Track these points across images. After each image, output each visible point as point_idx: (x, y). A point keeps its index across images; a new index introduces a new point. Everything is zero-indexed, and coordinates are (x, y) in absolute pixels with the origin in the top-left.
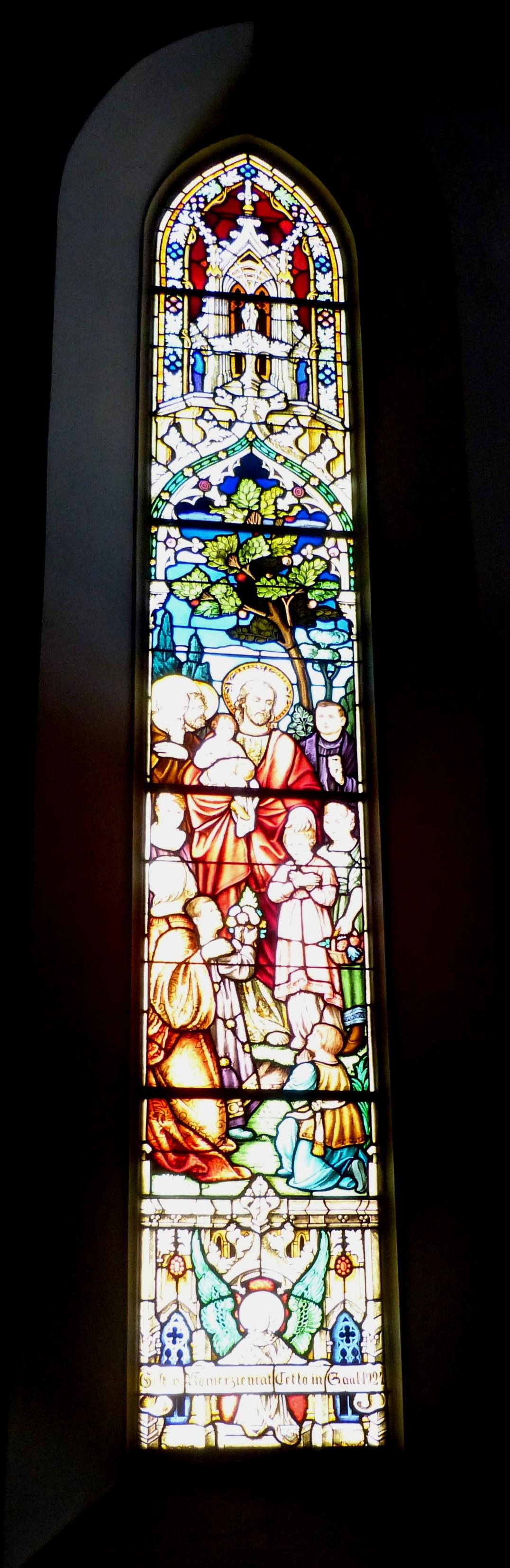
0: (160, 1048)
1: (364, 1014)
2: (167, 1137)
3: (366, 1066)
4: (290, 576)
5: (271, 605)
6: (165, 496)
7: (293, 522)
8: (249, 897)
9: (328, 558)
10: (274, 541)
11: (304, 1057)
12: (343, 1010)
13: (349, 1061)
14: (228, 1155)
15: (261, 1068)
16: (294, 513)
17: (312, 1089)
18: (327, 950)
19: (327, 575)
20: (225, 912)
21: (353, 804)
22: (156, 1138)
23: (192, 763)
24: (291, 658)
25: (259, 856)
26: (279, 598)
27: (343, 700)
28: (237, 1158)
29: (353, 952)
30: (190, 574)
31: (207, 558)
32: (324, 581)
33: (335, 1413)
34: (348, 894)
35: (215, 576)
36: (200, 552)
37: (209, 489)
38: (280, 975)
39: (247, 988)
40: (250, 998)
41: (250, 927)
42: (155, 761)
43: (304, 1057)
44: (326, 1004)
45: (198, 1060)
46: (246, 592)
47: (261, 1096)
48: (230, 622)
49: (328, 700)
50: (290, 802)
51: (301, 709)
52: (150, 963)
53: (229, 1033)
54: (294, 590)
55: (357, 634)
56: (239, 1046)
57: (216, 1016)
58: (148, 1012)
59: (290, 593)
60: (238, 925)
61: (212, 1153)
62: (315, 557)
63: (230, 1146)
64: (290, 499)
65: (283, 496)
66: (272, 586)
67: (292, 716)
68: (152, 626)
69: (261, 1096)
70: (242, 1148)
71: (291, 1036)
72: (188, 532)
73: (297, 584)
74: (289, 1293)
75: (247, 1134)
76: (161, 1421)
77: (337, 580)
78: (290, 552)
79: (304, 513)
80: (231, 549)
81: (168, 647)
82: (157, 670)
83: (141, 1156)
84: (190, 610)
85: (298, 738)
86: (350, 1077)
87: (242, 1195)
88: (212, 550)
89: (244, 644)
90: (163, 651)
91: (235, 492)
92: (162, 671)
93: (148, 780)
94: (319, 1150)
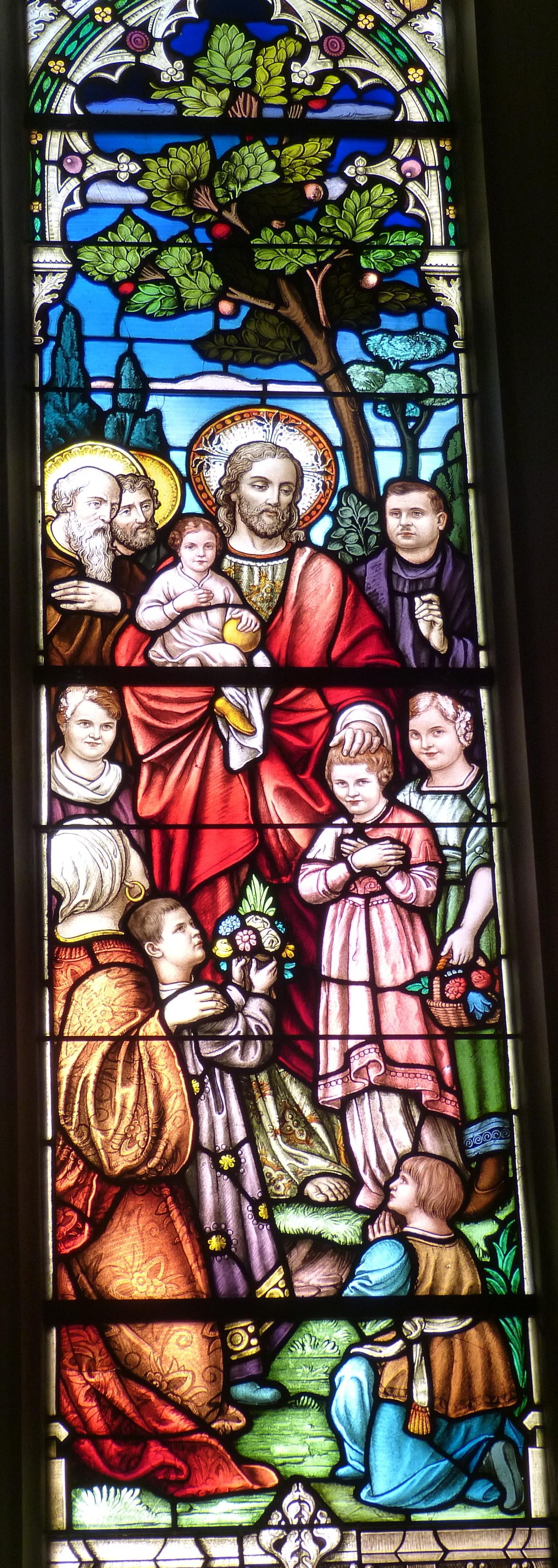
0: (82, 1218)
1: (506, 1132)
2: (99, 1405)
3: (514, 1241)
4: (322, 223)
5: (284, 286)
6: (57, 67)
7: (325, 109)
8: (257, 895)
9: (398, 180)
10: (286, 150)
11: (382, 1227)
12: (460, 1124)
13: (478, 1233)
14: (230, 1440)
15: (294, 1253)
16: (326, 90)
17: (403, 1293)
18: (424, 1000)
19: (400, 216)
20: (209, 928)
21: (467, 693)
22: (78, 1409)
23: (132, 621)
24: (328, 395)
25: (278, 810)
26: (301, 270)
27: (441, 478)
28: (250, 1445)
29: (476, 1000)
30: (114, 228)
31: (148, 192)
32: (393, 229)
34: (465, 881)
35: (165, 229)
36: (133, 181)
37: (149, 49)
38: (331, 1056)
39: (260, 1086)
40: (269, 1108)
41: (261, 957)
42: (55, 618)
43: (382, 1227)
44: (427, 1114)
45: (160, 1242)
46: (231, 258)
47: (297, 1312)
48: (200, 325)
49: (408, 479)
50: (336, 695)
51: (353, 500)
52: (58, 1040)
53: (226, 1184)
54: (330, 252)
55: (465, 338)
56: (247, 1207)
57: (197, 1146)
58: (53, 1143)
59: (323, 258)
60: (237, 953)
61: (197, 1437)
62: (374, 180)
63: (234, 1420)
64: (315, 62)
65: (302, 57)
66: (286, 246)
67: (334, 515)
68: (39, 340)
69: (297, 1312)
70: (261, 1423)
71: (355, 1184)
72: (107, 141)
73: (336, 238)
75: (267, 1394)
77: (422, 226)
78: (319, 173)
79: (347, 90)
80: (198, 171)
81: (73, 382)
82: (52, 431)
83: (47, 1447)
84: (115, 303)
85: (349, 560)
86: (480, 1267)
87: (262, 1524)
88: (157, 177)
89: (232, 369)
90: (63, 390)
91: (203, 51)
92: (62, 432)
93: (41, 659)
94: (418, 1424)
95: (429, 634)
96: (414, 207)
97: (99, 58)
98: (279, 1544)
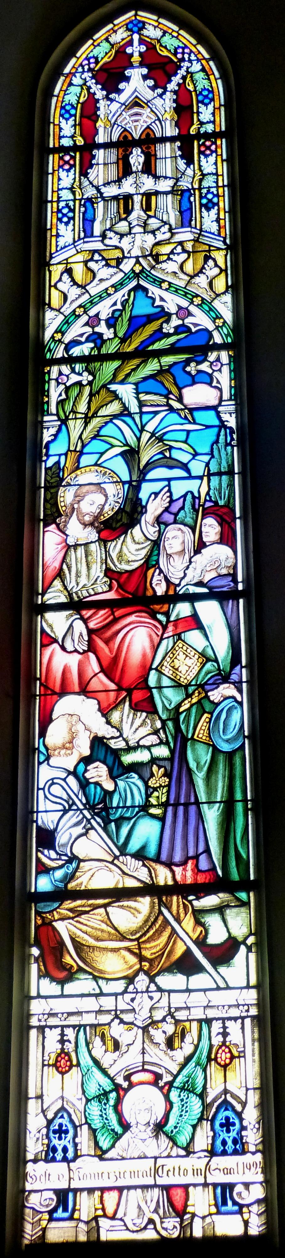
6: (58, 336)
33: (216, 1205)
74: (170, 1084)
76: (46, 1216)
83: (29, 959)
95: (130, 383)
97: (78, 329)
98: (133, 1000)
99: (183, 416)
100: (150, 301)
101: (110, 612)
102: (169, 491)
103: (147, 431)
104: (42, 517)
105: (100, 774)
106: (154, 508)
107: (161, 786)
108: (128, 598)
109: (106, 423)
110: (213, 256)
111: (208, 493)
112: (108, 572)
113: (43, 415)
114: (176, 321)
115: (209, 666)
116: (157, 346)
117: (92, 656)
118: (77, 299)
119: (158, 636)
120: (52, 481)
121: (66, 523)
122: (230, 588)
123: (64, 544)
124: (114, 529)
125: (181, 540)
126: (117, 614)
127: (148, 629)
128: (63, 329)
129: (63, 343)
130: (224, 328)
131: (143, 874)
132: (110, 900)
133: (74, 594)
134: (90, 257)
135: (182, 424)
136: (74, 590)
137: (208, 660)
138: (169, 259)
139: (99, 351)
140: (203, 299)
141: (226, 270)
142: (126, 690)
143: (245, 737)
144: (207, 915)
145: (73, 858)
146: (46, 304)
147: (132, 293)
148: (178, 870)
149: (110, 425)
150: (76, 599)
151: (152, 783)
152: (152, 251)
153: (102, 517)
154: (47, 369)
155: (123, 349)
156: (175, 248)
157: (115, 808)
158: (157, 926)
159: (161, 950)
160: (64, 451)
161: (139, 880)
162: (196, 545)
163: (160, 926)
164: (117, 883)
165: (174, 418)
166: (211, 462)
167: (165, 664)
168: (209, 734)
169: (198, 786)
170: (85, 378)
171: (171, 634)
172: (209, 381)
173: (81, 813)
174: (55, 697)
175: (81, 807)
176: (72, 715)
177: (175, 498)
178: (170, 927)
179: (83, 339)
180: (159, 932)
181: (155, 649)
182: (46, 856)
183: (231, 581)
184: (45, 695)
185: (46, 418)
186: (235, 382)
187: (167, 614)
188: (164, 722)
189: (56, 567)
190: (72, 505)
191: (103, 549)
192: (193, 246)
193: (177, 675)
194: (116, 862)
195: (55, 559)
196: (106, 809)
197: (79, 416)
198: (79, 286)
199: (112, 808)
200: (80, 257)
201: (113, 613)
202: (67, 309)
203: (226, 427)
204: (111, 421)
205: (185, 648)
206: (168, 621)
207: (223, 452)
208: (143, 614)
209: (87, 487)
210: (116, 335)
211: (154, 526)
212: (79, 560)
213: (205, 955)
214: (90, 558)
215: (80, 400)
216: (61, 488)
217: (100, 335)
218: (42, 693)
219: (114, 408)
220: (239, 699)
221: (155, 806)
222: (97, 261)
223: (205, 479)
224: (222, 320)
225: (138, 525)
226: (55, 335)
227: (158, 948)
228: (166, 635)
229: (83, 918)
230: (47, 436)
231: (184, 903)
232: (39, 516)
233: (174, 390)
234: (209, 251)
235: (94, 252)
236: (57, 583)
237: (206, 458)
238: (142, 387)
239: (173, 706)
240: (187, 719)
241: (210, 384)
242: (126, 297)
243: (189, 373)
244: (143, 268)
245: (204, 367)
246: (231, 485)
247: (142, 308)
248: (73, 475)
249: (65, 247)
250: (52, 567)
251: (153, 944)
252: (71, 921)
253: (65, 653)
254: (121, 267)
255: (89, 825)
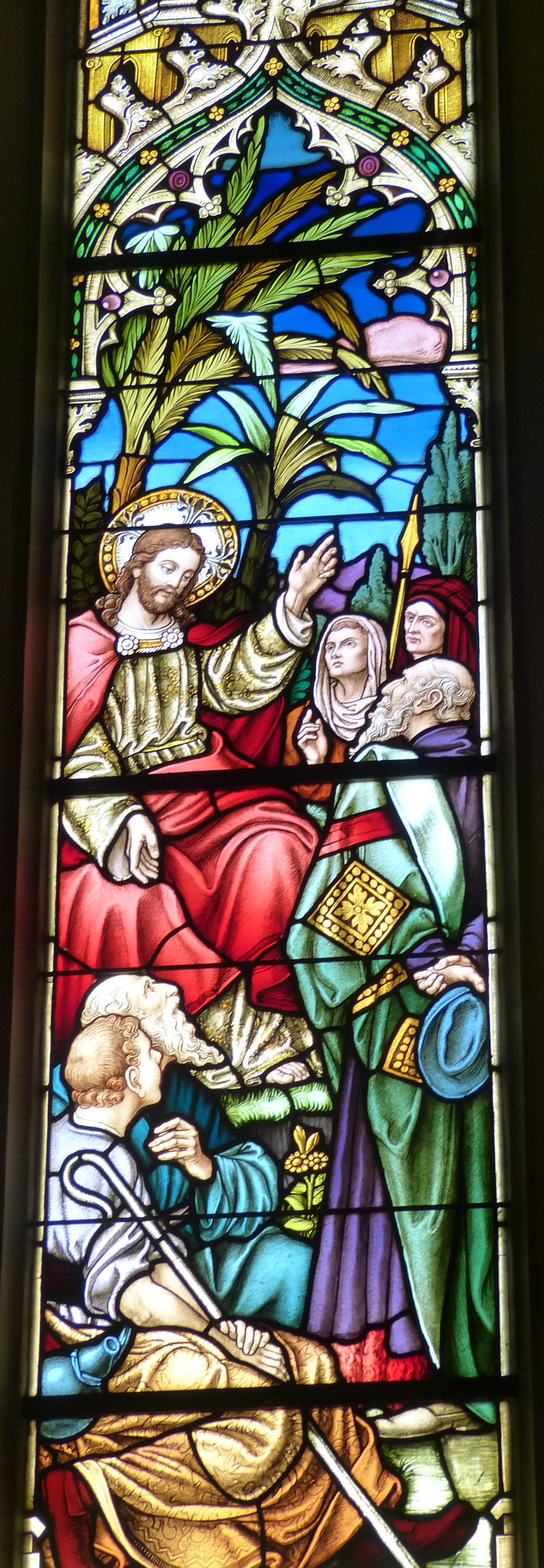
6: (103, 210)
37: (189, 186)
95: (254, 313)
96: (439, 315)
99: (366, 384)
100: (300, 138)
101: (207, 800)
102: (336, 543)
103: (290, 416)
104: (64, 596)
105: (181, 1142)
106: (302, 580)
107: (310, 1171)
108: (246, 770)
109: (204, 398)
110: (434, 42)
111: (418, 550)
112: (204, 714)
113: (69, 379)
114: (353, 183)
115: (416, 916)
116: (313, 234)
117: (168, 893)
118: (143, 131)
119: (308, 850)
120: (87, 518)
121: (116, 608)
122: (464, 751)
123: (110, 653)
124: (217, 624)
125: (357, 650)
126: (223, 802)
127: (287, 836)
128: (114, 194)
129: (112, 224)
130: (457, 199)
131: (271, 1360)
132: (199, 1415)
133: (131, 760)
134: (172, 40)
135: (365, 402)
136: (131, 752)
137: (415, 903)
138: (341, 47)
139: (190, 243)
140: (412, 135)
141: (463, 73)
142: (238, 965)
143: (491, 1069)
144: (408, 1451)
145: (121, 1323)
146: (77, 141)
147: (262, 120)
148: (346, 1353)
149: (212, 401)
150: (135, 770)
151: (292, 1164)
152: (304, 29)
153: (193, 597)
154: (78, 280)
155: (241, 239)
156: (354, 24)
157: (211, 1216)
158: (300, 1474)
159: (307, 1525)
160: (111, 455)
161: (262, 1373)
162: (392, 658)
163: (306, 1473)
164: (216, 1377)
165: (347, 386)
166: (426, 483)
167: (324, 910)
168: (416, 1061)
169: (391, 1172)
170: (159, 300)
171: (336, 847)
172: (422, 310)
173: (141, 1226)
174: (88, 978)
175: (140, 1214)
176: (123, 1017)
177: (348, 557)
178: (326, 1477)
179: (156, 218)
180: (304, 1486)
181: (303, 879)
182: (62, 1318)
183: (465, 737)
184: (67, 973)
185: (76, 386)
186: (479, 314)
187: (329, 806)
188: (318, 1035)
189: (92, 704)
190: (129, 570)
191: (194, 666)
192: (393, 20)
193: (348, 934)
194: (212, 1333)
195: (90, 682)
196: (195, 1218)
197: (146, 381)
198: (147, 103)
199: (207, 1217)
200: (149, 42)
201: (213, 802)
202: (122, 152)
203: (458, 409)
204: (213, 393)
205: (365, 878)
206: (331, 820)
207: (451, 463)
208: (278, 805)
209: (162, 534)
210: (225, 210)
211: (301, 617)
212: (142, 686)
213: (404, 1539)
214: (165, 683)
215: (149, 346)
216: (125, 392)
217: (194, 209)
218: (61, 968)
219: (219, 365)
220: (481, 988)
221: (297, 1214)
222: (186, 51)
223: (413, 518)
224: (452, 181)
225: (269, 618)
226: (97, 207)
227: (301, 1523)
228: (325, 850)
229: (141, 1455)
230: (76, 424)
231: (357, 1424)
232: (59, 591)
233: (349, 329)
234: (428, 31)
235: (180, 29)
236: (95, 736)
237: (415, 475)
238: (280, 321)
239: (338, 1000)
240: (368, 1027)
241: (425, 317)
242: (249, 128)
243: (381, 293)
244: (286, 65)
245: (414, 280)
246: (468, 533)
247: (283, 152)
248: (132, 507)
249: (119, 18)
250: (85, 701)
251: (290, 1513)
252: (114, 1460)
253: (109, 885)
254: (238, 64)
255: (156, 1254)
